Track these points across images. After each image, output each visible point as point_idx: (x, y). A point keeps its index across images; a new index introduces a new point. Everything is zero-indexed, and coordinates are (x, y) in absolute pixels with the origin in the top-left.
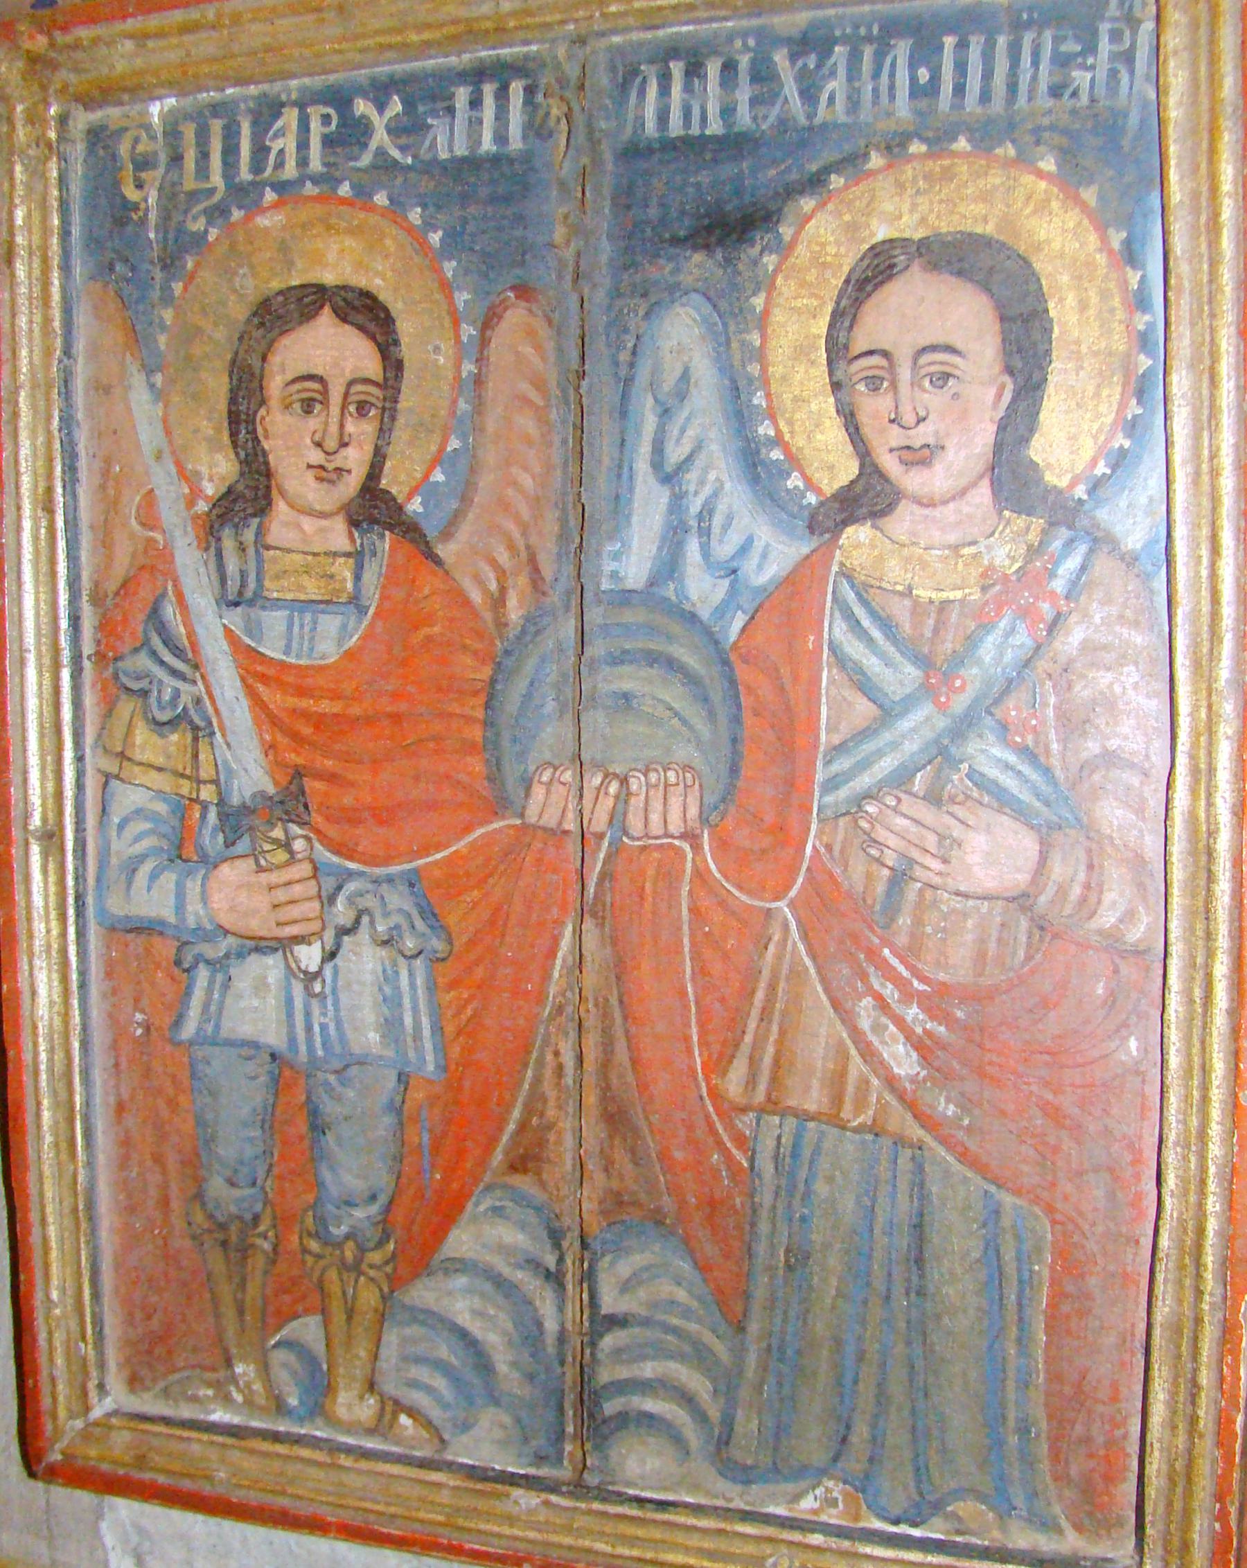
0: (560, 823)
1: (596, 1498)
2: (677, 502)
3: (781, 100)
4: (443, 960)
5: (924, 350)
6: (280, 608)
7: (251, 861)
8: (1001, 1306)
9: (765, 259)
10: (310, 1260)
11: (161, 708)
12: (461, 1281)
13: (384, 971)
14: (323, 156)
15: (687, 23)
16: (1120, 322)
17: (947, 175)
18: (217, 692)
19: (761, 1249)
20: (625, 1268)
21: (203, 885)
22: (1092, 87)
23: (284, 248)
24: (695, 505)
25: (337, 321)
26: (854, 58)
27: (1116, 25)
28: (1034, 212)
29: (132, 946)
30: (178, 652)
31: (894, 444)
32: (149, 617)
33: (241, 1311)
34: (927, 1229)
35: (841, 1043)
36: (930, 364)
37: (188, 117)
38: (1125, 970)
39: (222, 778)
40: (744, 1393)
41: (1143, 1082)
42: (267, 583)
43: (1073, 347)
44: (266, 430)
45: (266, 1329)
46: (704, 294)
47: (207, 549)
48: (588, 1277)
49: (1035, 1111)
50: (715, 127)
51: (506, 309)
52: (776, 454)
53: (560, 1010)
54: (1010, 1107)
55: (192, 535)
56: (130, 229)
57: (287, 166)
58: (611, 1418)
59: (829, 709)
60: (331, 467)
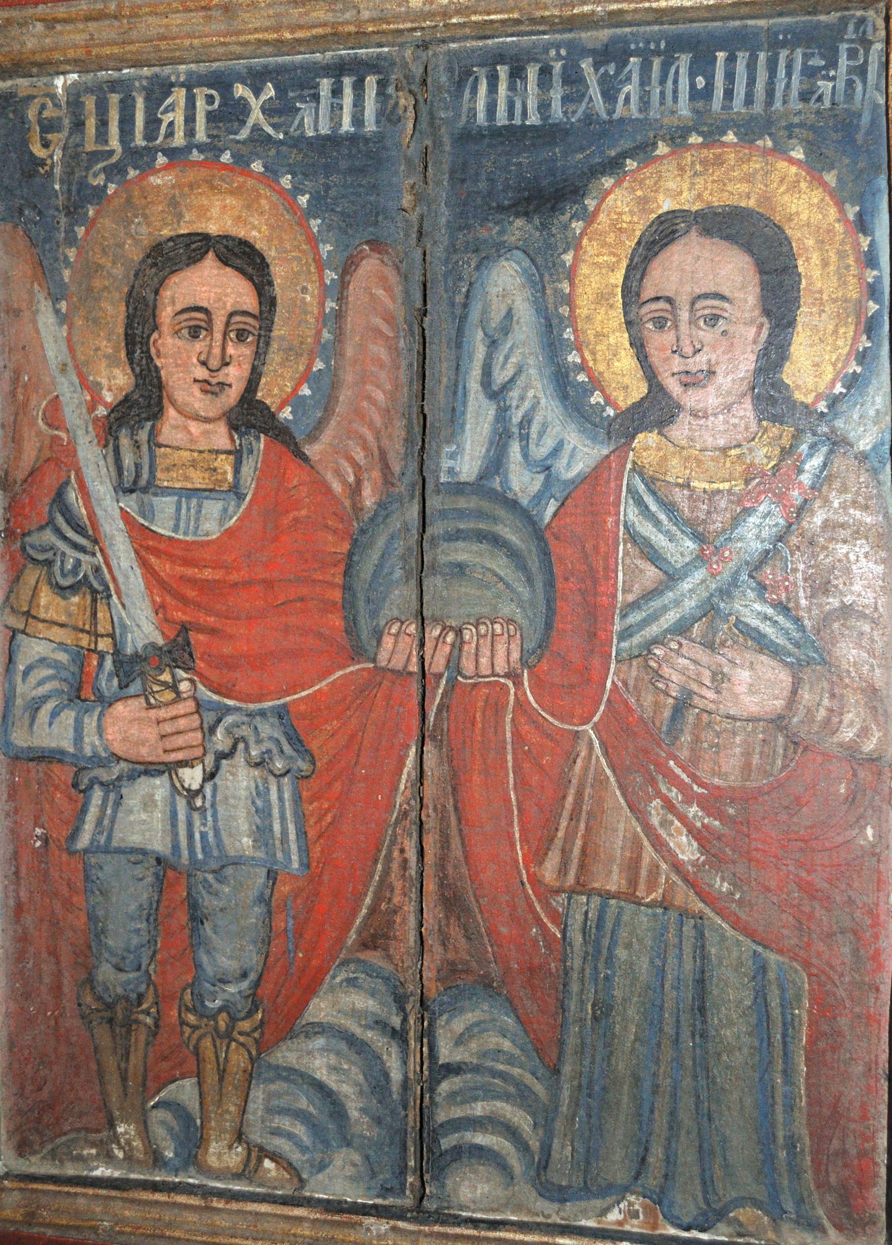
0: (406, 666)
1: (436, 1222)
2: (503, 413)
3: (586, 100)
4: (307, 777)
5: (699, 297)
6: (169, 495)
7: (142, 700)
8: (770, 1044)
9: (573, 225)
10: (187, 1031)
11: (64, 575)
12: (320, 1042)
13: (257, 787)
14: (207, 129)
15: (512, 35)
16: (854, 276)
17: (719, 161)
18: (114, 563)
19: (573, 1005)
20: (459, 1025)
21: (99, 719)
22: (833, 93)
23: (173, 203)
24: (517, 417)
25: (219, 264)
26: (646, 67)
27: (853, 46)
28: (787, 190)
29: (33, 774)
30: (79, 529)
31: (675, 370)
32: (54, 501)
33: (124, 1079)
34: (707, 982)
35: (636, 836)
36: (704, 308)
37: (89, 90)
38: (861, 774)
39: (118, 631)
40: (559, 1125)
41: (879, 861)
42: (159, 475)
43: (817, 296)
44: (158, 351)
45: (146, 1092)
46: (525, 252)
47: (105, 446)
48: (427, 1035)
49: (792, 886)
50: (533, 119)
51: (362, 259)
52: (582, 377)
53: (405, 814)
54: (773, 884)
55: (93, 433)
56: (37, 180)
57: (176, 136)
58: (446, 1151)
59: (624, 575)
60: (214, 381)
